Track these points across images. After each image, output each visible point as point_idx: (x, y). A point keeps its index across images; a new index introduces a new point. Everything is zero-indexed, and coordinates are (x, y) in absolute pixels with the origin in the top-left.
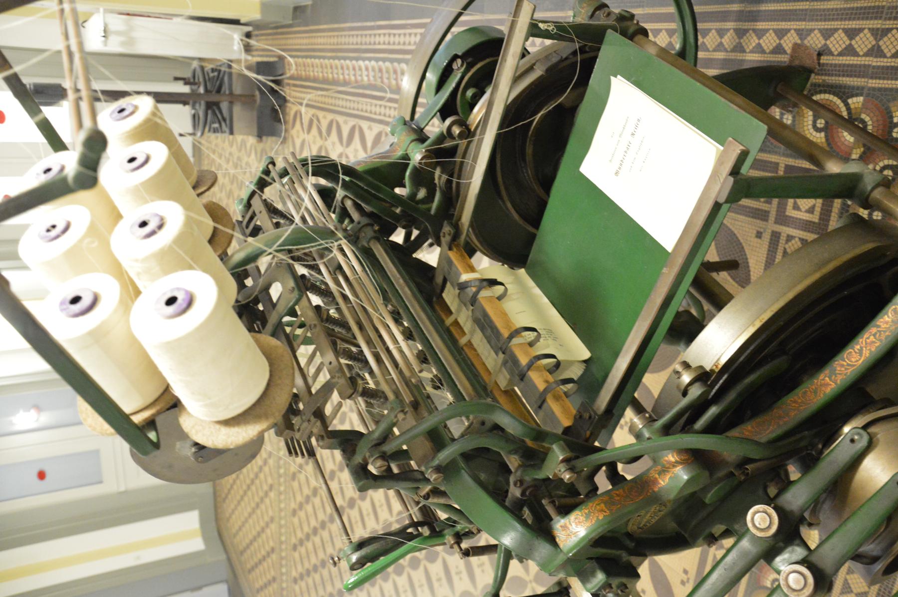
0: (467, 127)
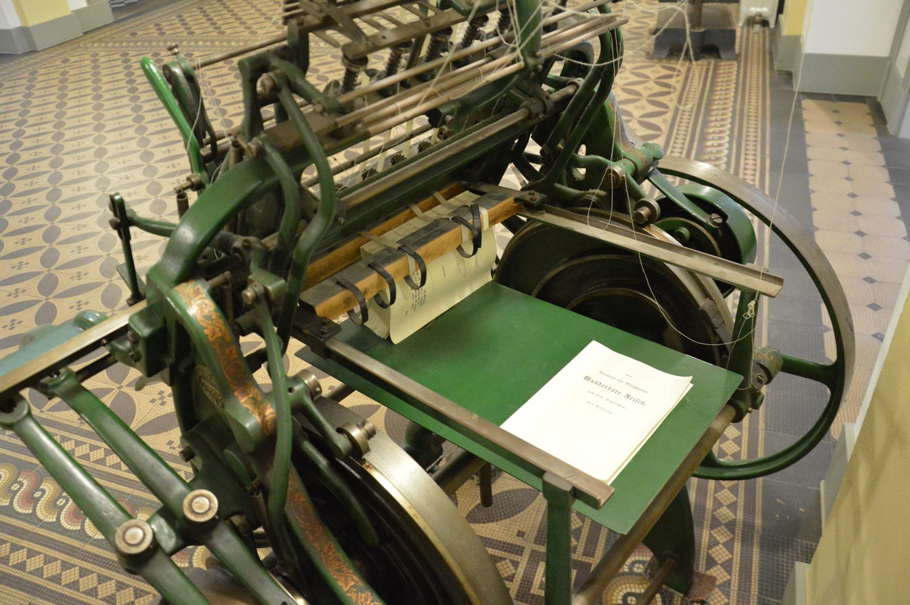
0: (647, 224)
